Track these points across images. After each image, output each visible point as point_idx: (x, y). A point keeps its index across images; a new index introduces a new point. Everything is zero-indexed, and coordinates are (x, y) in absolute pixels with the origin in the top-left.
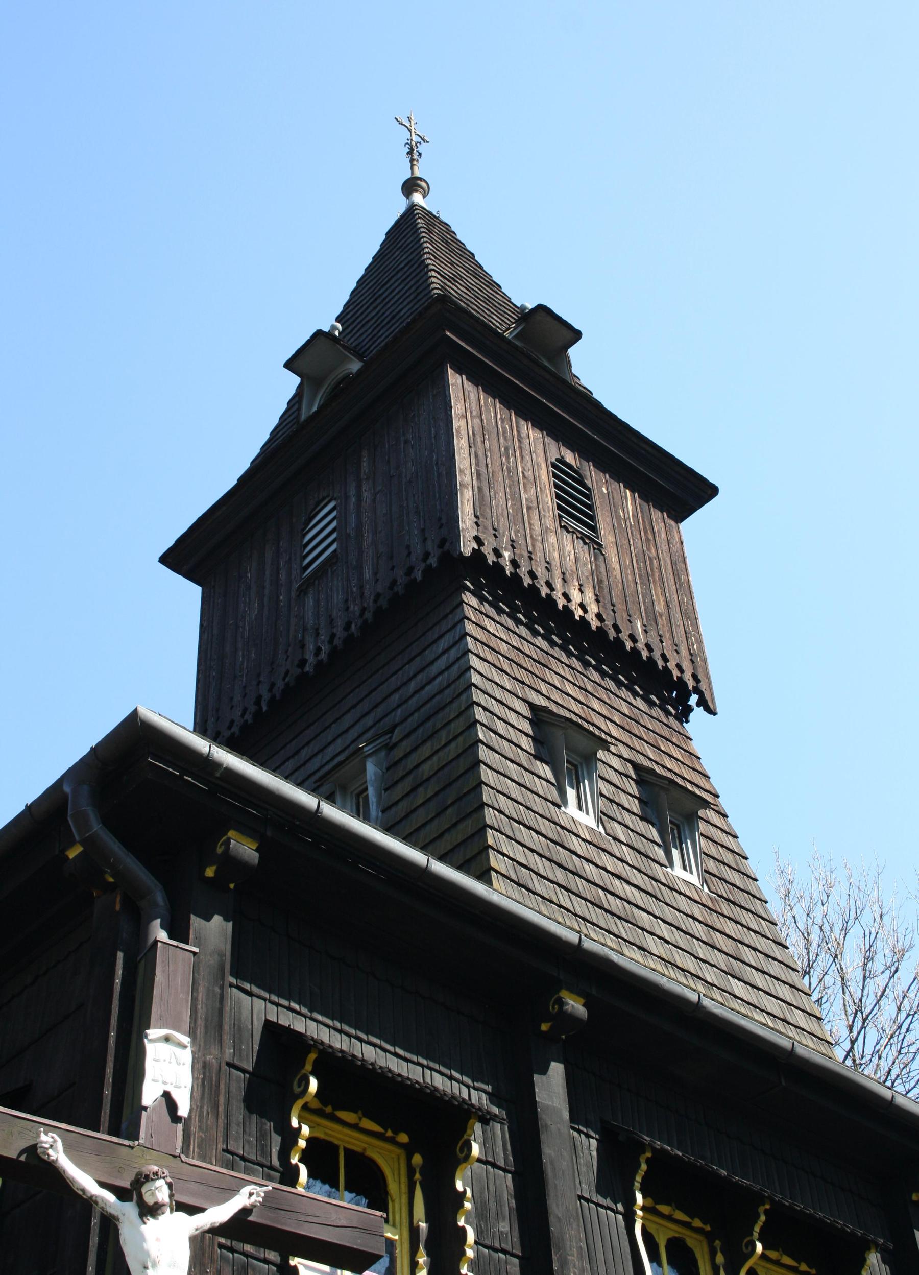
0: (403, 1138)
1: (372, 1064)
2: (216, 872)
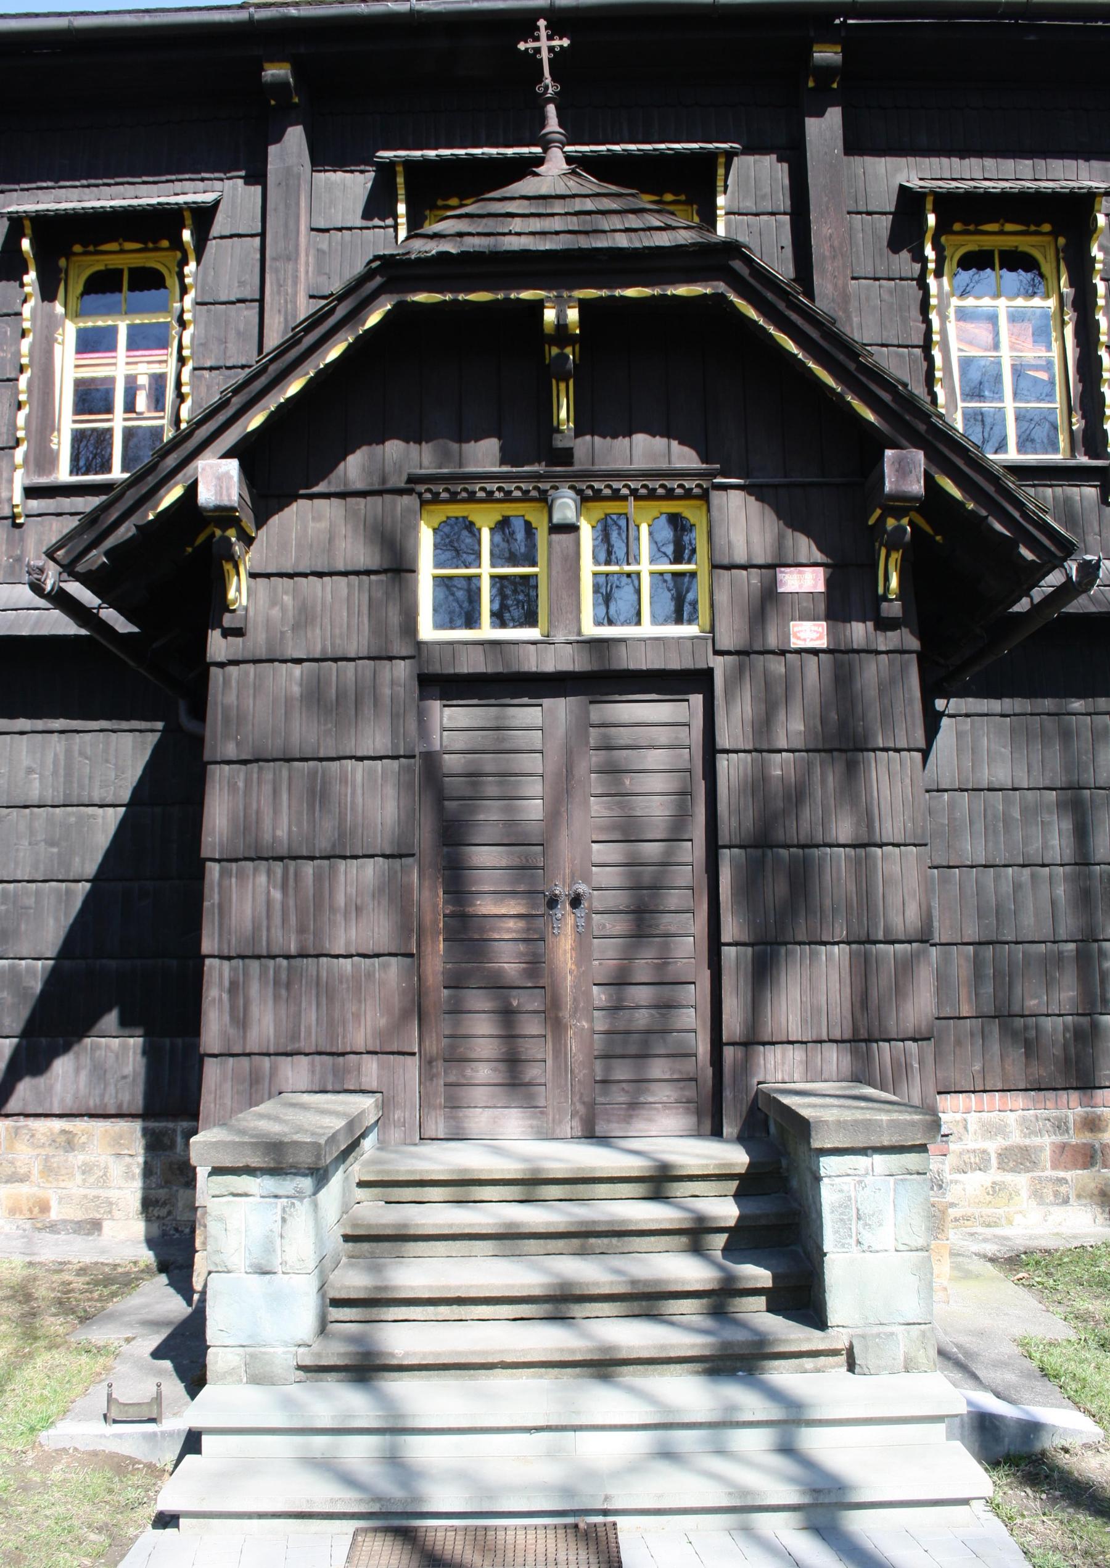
0: (1046, 227)
2: (815, 81)
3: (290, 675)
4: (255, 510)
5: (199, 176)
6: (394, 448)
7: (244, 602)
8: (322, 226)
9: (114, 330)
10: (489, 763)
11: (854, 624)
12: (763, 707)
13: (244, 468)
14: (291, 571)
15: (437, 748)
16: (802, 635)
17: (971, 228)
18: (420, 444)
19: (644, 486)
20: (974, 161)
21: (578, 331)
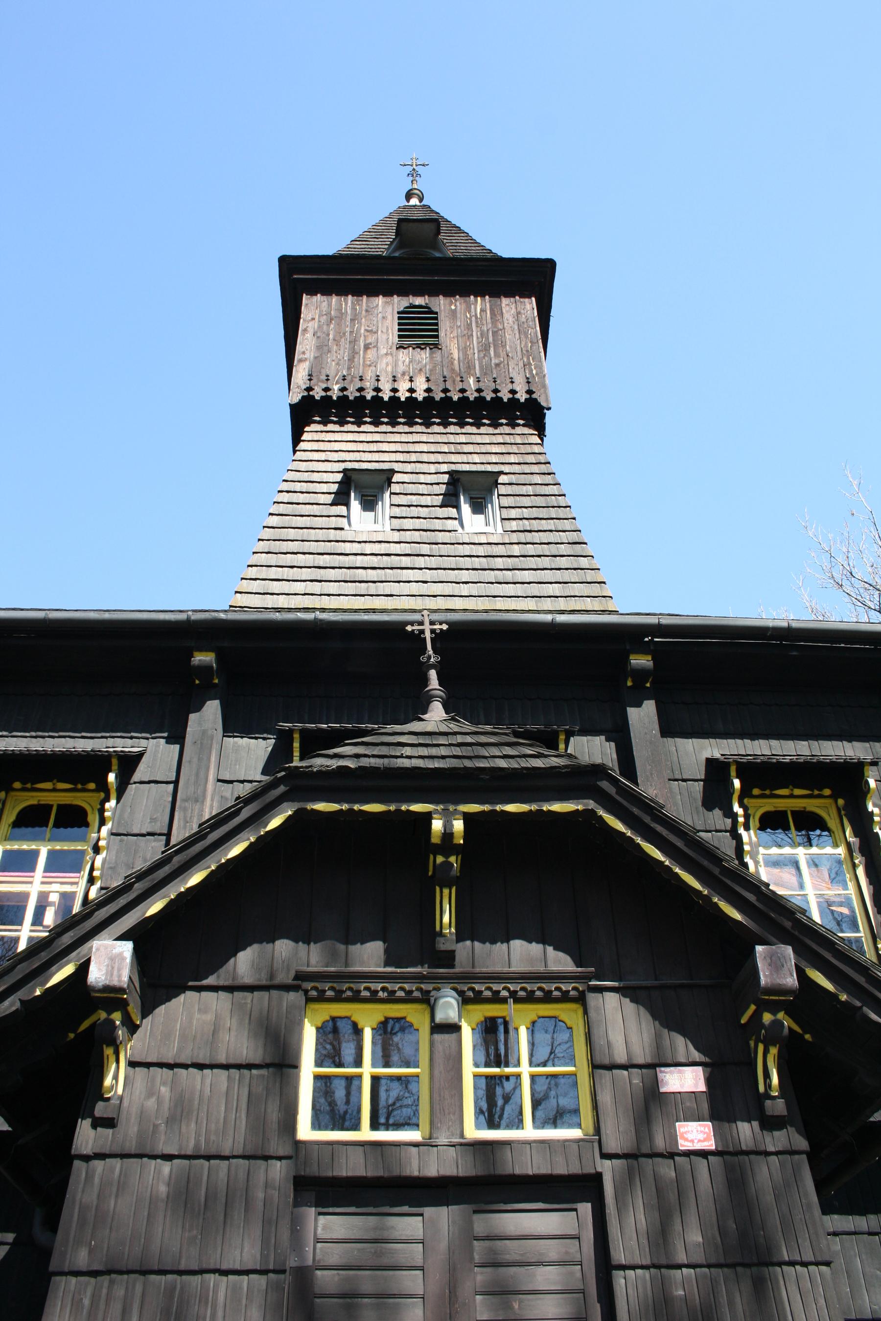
0: (827, 792)
1: (92, 751)
2: (633, 681)
3: (158, 1172)
4: (142, 997)
5: (129, 735)
6: (283, 947)
7: (120, 1091)
8: (227, 778)
9: (35, 854)
10: (367, 1281)
11: (739, 1124)
12: (657, 1215)
13: (137, 952)
14: (171, 1061)
15: (310, 1262)
16: (690, 1136)
17: (767, 792)
18: (309, 944)
19: (523, 989)
20: (762, 742)
21: (462, 842)
